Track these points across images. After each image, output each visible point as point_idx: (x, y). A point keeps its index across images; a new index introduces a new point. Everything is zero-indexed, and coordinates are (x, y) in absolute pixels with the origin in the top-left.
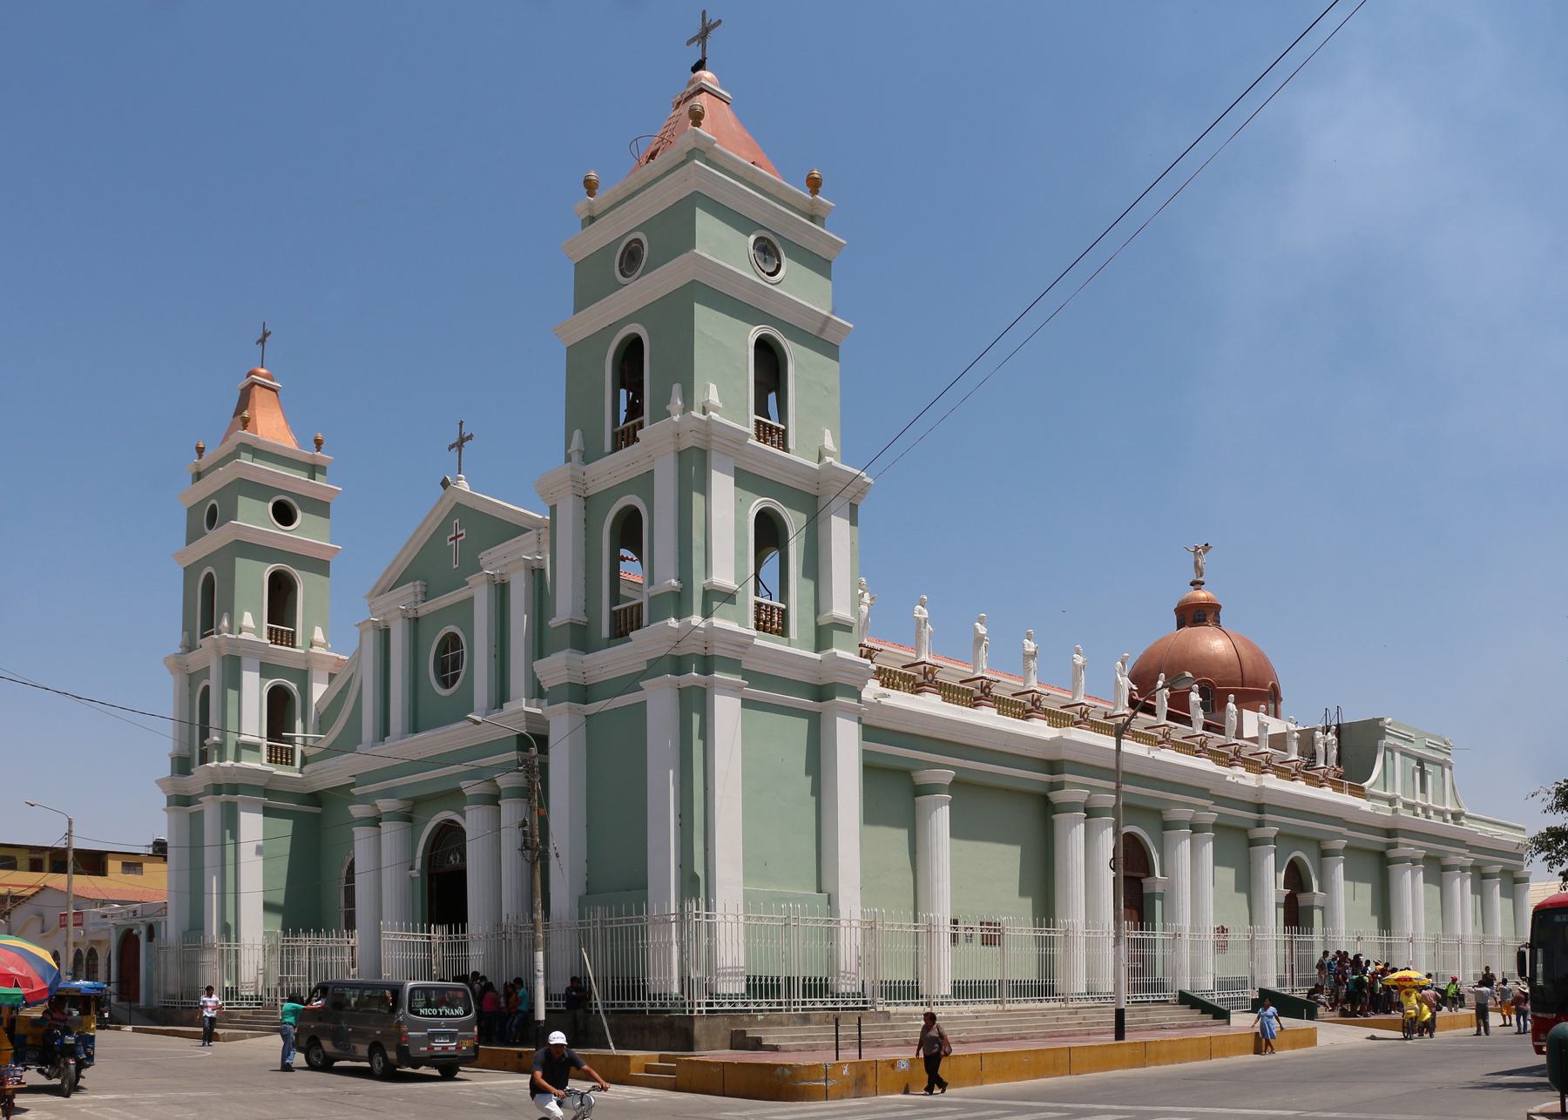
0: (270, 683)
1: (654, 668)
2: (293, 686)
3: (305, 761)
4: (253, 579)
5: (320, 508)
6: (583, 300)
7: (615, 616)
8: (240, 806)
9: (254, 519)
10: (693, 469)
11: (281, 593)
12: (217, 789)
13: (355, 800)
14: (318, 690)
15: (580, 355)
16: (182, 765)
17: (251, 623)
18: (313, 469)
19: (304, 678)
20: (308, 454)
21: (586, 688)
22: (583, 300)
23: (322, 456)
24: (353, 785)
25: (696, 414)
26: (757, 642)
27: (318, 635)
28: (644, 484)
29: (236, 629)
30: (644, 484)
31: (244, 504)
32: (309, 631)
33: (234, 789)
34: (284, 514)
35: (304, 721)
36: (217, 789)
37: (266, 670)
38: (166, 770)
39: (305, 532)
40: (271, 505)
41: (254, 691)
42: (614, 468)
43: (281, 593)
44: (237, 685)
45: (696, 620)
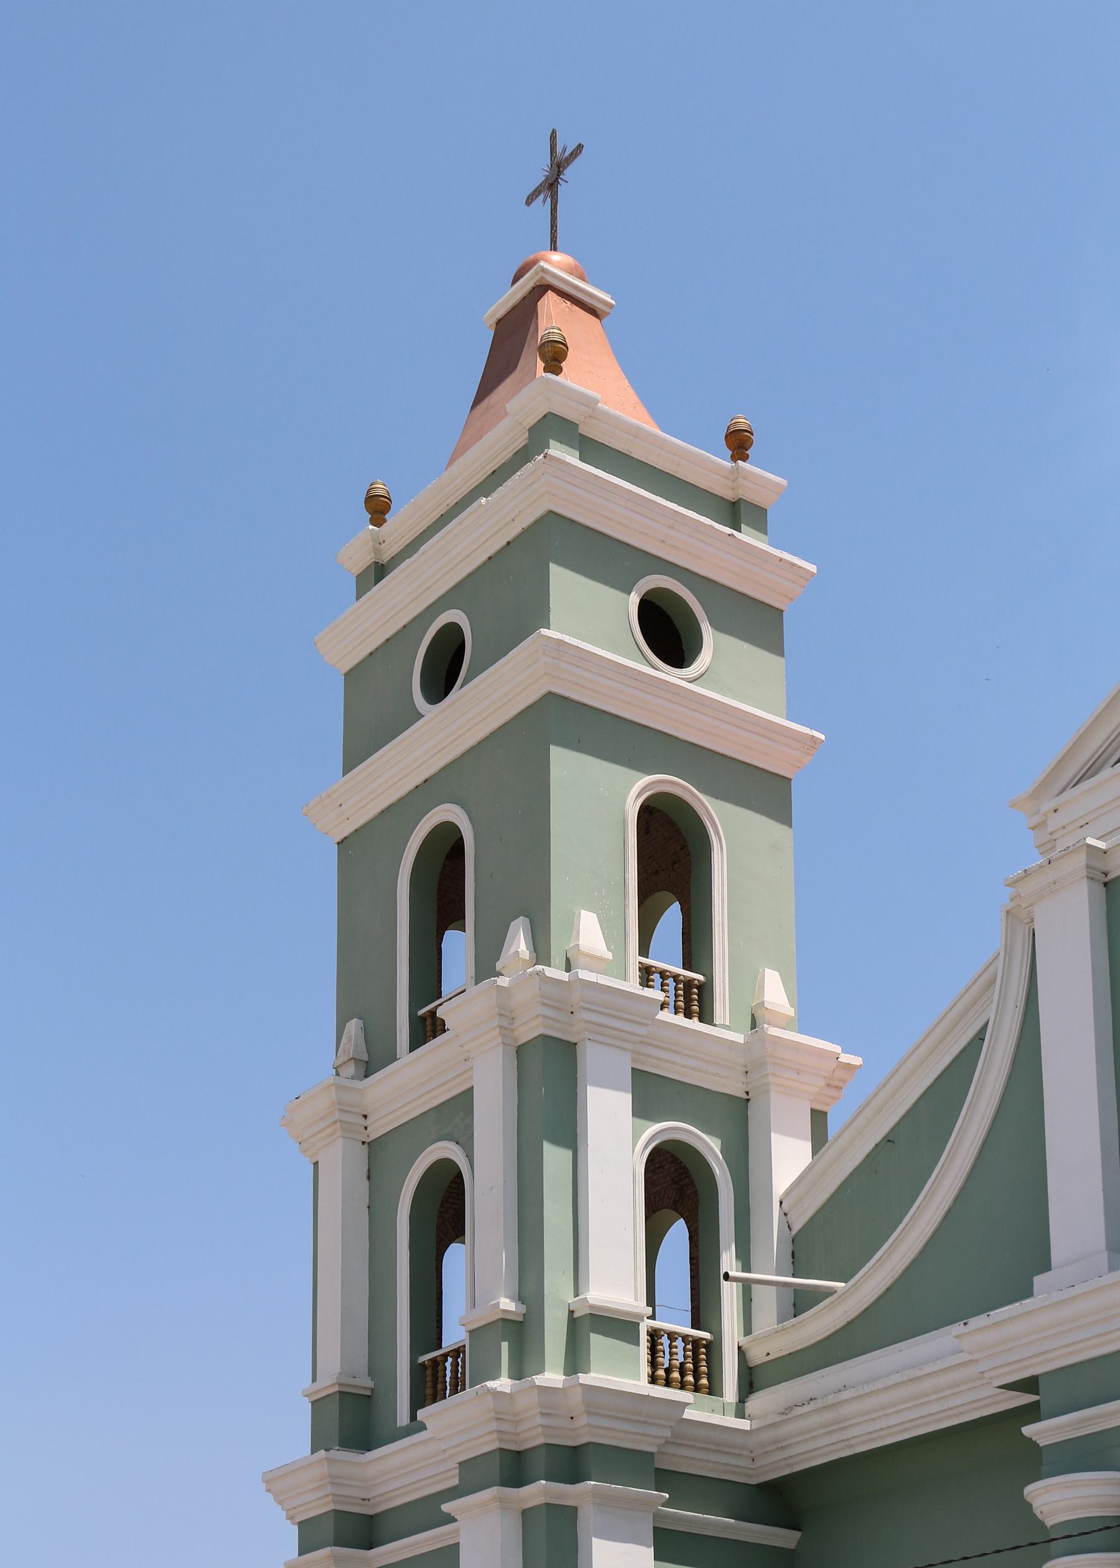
0: (653, 1131)
1: (473, 1476)
2: (711, 1146)
3: (751, 1380)
4: (594, 809)
5: (759, 622)
6: (359, 746)
7: (417, 1371)
8: (588, 1518)
9: (589, 628)
10: (549, 1081)
11: (671, 857)
12: (513, 1467)
13: (1038, 1462)
14: (788, 1160)
15: (359, 851)
16: (353, 1420)
17: (596, 930)
18: (735, 512)
19: (736, 1117)
20: (711, 465)
21: (575, 1451)
22: (359, 746)
23: (759, 477)
24: (1032, 1413)
25: (555, 973)
26: (689, 1414)
27: (775, 993)
28: (455, 1114)
29: (557, 957)
30: (455, 1114)
31: (565, 584)
32: (748, 981)
33: (571, 1463)
34: (667, 633)
35: (745, 1259)
36: (513, 1467)
37: (651, 1093)
38: (292, 1437)
39: (728, 687)
40: (634, 600)
41: (615, 1142)
42: (411, 1083)
43: (671, 857)
44: (568, 1130)
45: (552, 1377)
